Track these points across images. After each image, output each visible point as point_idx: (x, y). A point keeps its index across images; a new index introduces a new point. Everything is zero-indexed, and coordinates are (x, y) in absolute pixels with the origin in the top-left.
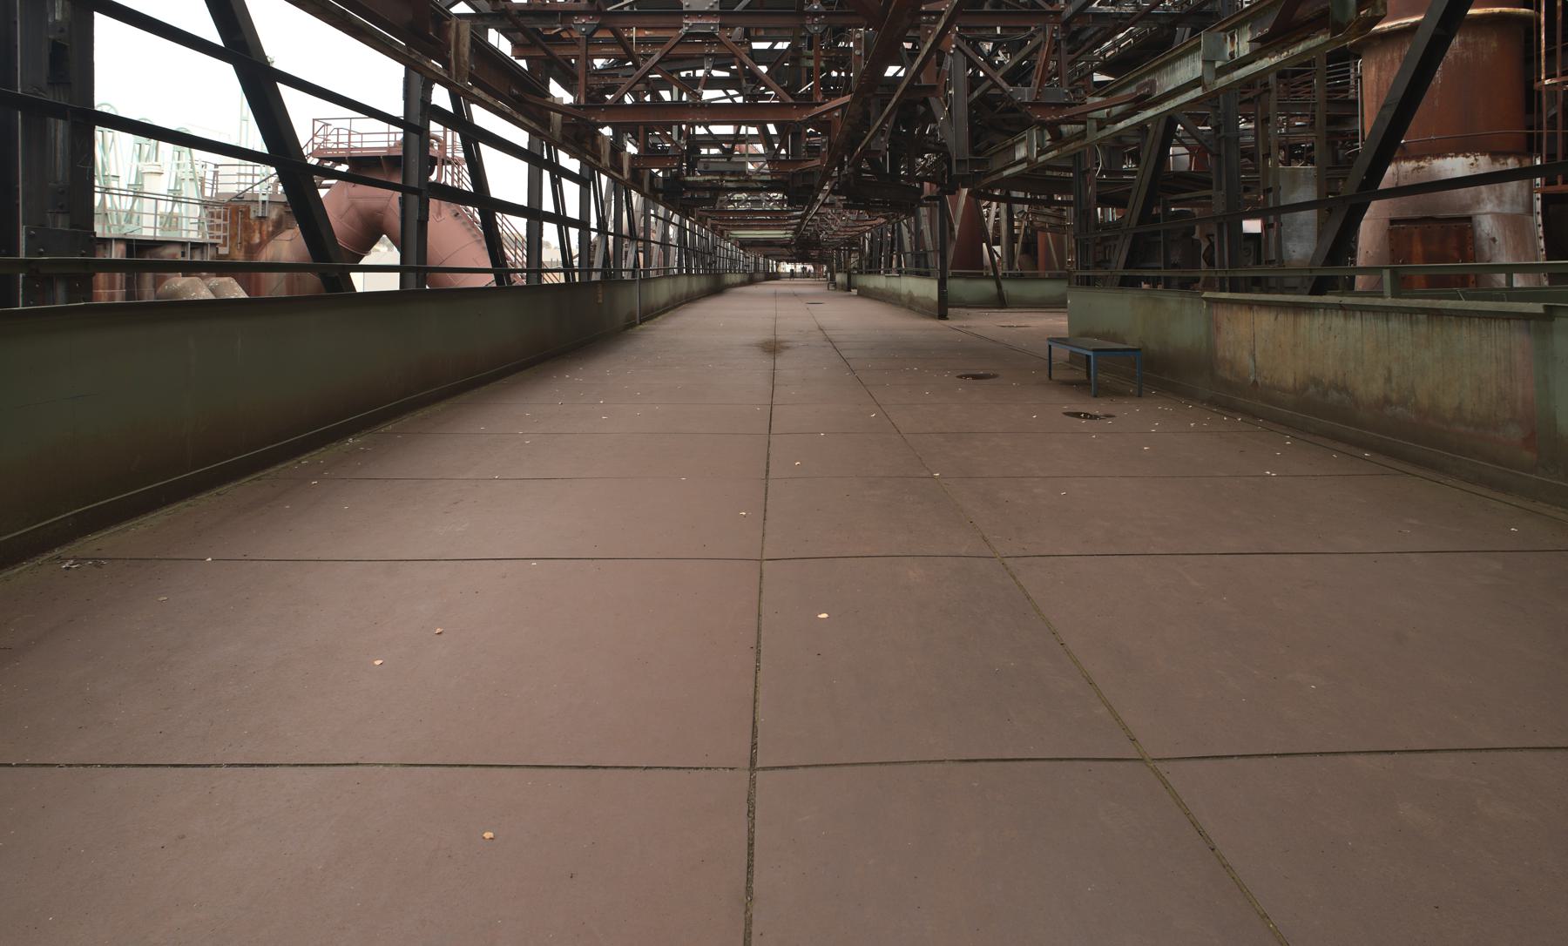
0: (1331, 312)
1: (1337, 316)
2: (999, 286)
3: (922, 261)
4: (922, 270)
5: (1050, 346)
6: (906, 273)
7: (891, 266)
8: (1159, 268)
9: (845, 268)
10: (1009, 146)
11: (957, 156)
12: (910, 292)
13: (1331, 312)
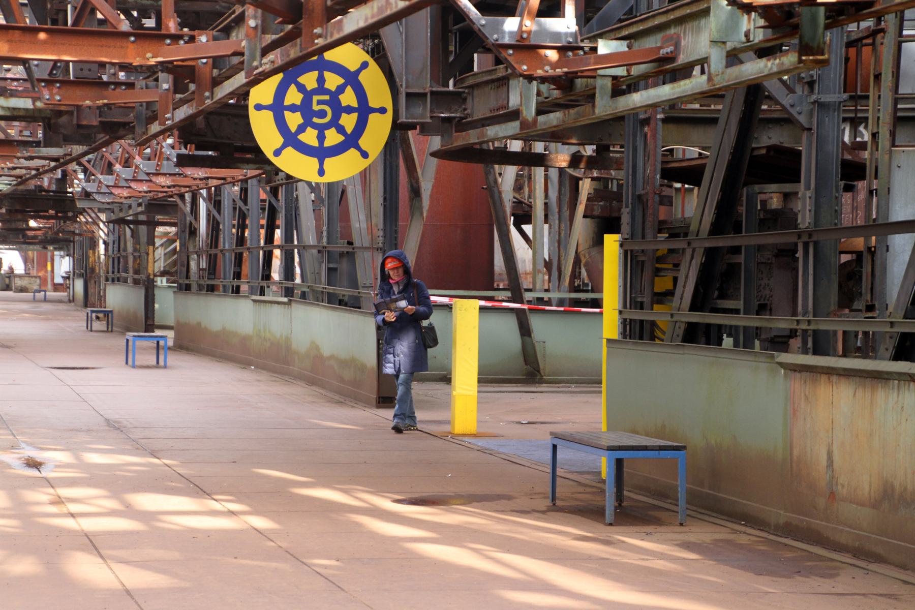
0: (905, 385)
1: (909, 390)
2: (525, 330)
3: (344, 266)
4: (344, 291)
5: (555, 447)
6: (304, 295)
7: (267, 277)
8: (737, 311)
9: (137, 272)
10: (499, 80)
11: (407, 87)
12: (313, 343)
13: (905, 385)
